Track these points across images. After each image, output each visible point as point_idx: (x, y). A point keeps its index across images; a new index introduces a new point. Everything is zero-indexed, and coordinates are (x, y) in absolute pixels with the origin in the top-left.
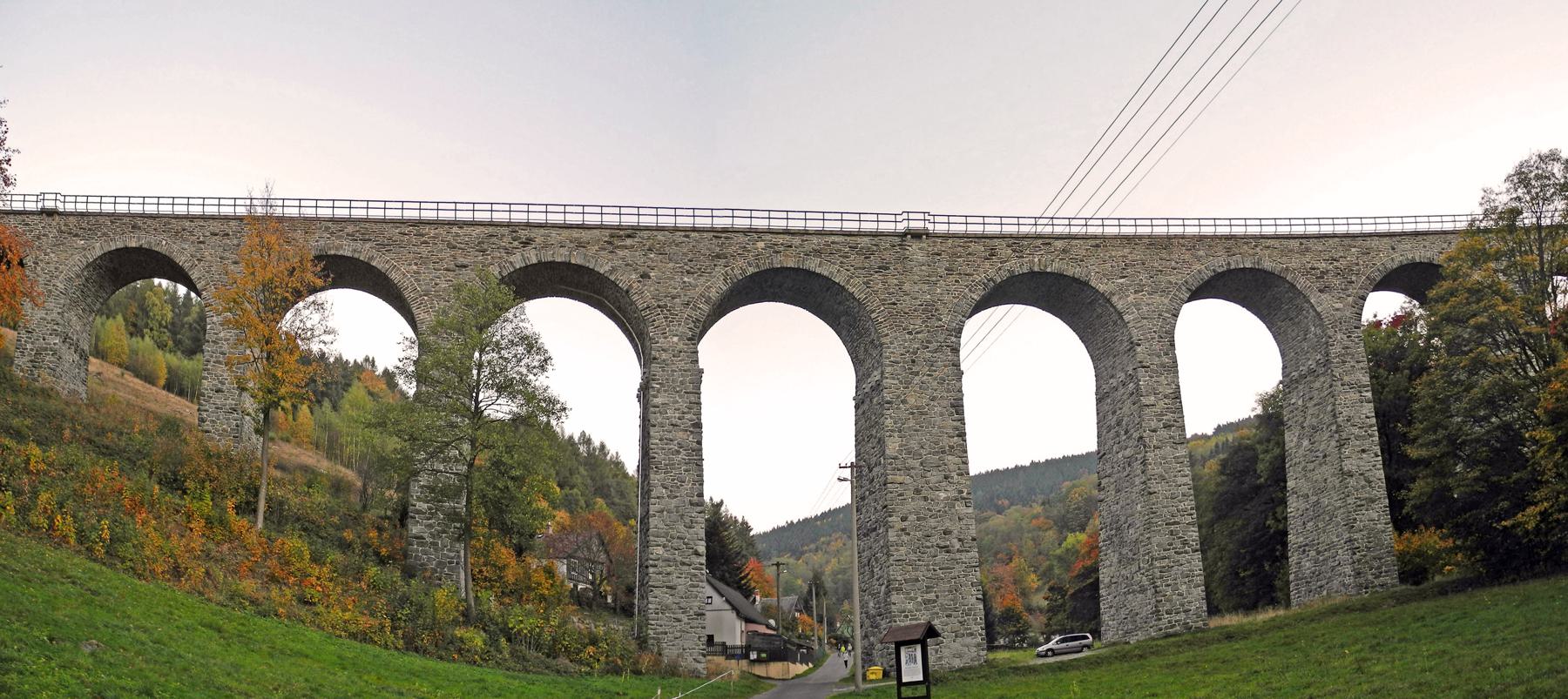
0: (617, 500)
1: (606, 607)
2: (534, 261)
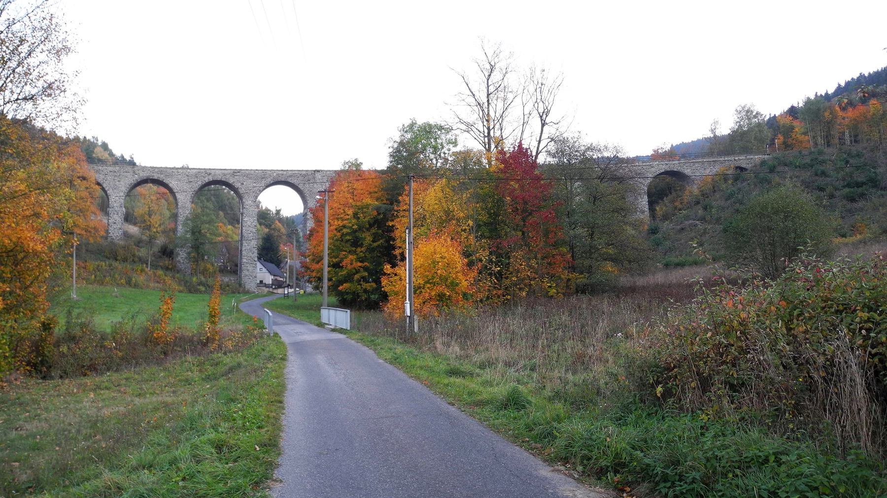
0: (229, 212)
1: (228, 271)
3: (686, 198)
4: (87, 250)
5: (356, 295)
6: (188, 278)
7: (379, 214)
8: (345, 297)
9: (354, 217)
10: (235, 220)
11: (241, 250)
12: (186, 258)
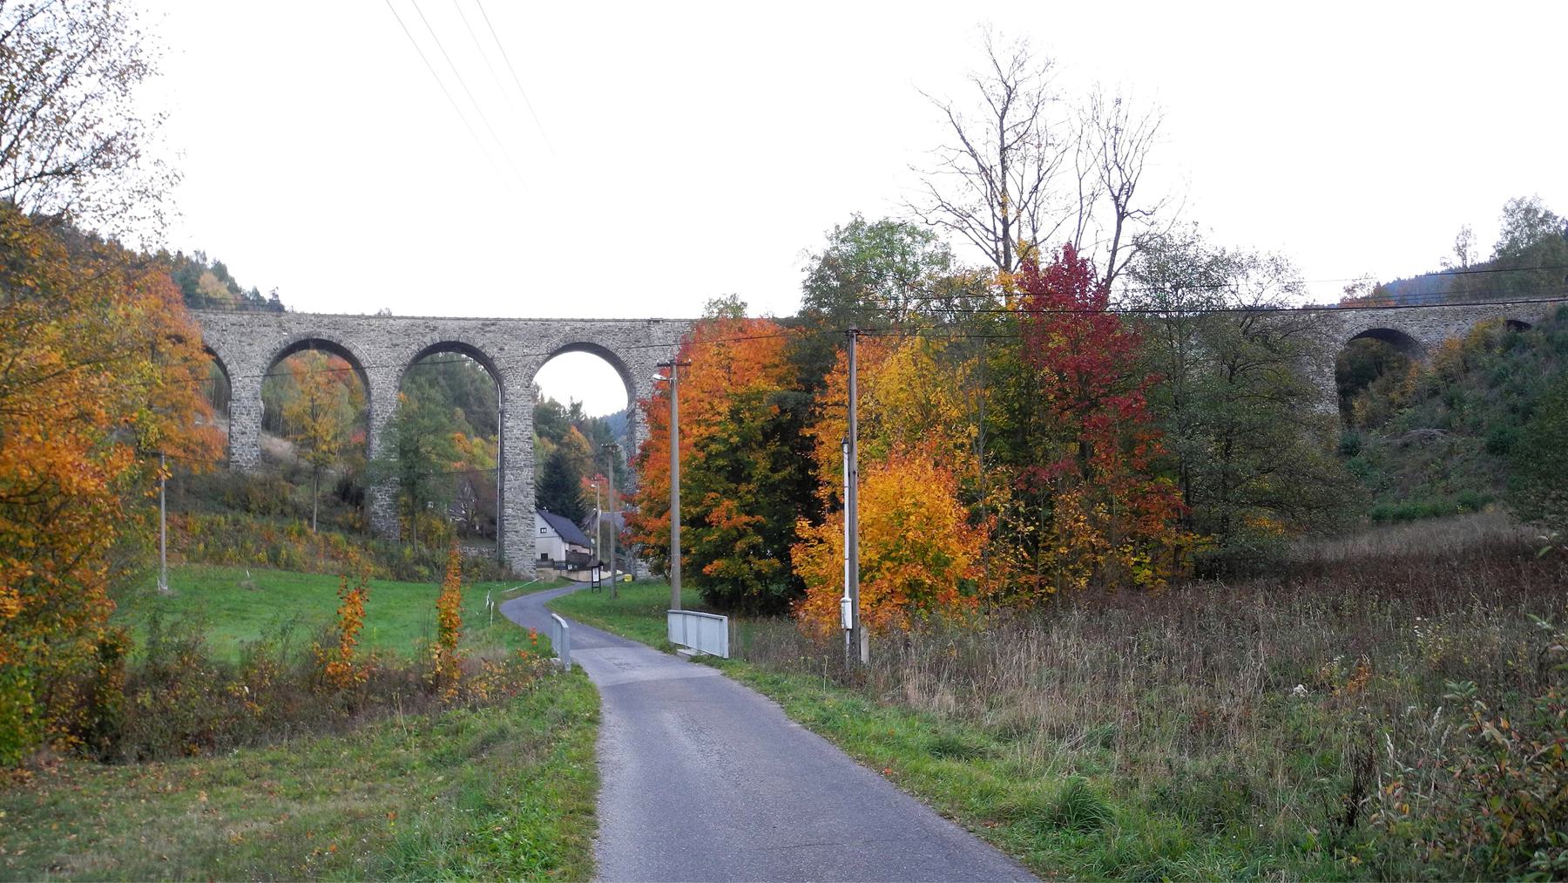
0: (475, 408)
1: (475, 534)
2: (438, 341)
3: (1412, 383)
4: (188, 491)
5: (739, 584)
6: (394, 549)
7: (783, 412)
8: (717, 589)
9: (732, 418)
10: (488, 426)
11: (502, 490)
12: (390, 507)
